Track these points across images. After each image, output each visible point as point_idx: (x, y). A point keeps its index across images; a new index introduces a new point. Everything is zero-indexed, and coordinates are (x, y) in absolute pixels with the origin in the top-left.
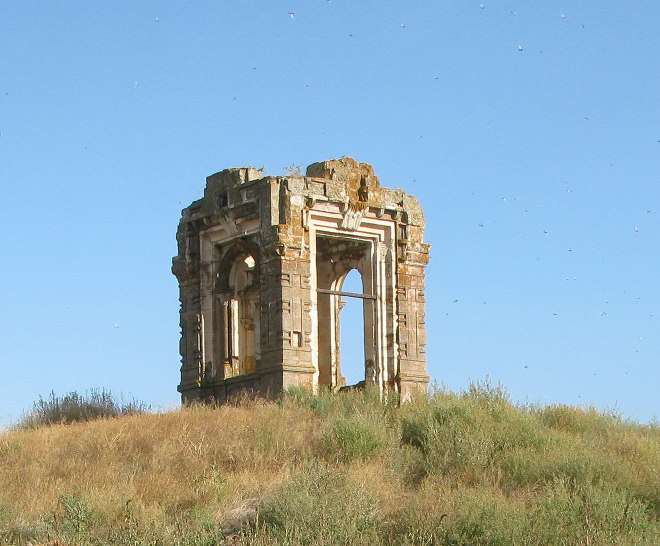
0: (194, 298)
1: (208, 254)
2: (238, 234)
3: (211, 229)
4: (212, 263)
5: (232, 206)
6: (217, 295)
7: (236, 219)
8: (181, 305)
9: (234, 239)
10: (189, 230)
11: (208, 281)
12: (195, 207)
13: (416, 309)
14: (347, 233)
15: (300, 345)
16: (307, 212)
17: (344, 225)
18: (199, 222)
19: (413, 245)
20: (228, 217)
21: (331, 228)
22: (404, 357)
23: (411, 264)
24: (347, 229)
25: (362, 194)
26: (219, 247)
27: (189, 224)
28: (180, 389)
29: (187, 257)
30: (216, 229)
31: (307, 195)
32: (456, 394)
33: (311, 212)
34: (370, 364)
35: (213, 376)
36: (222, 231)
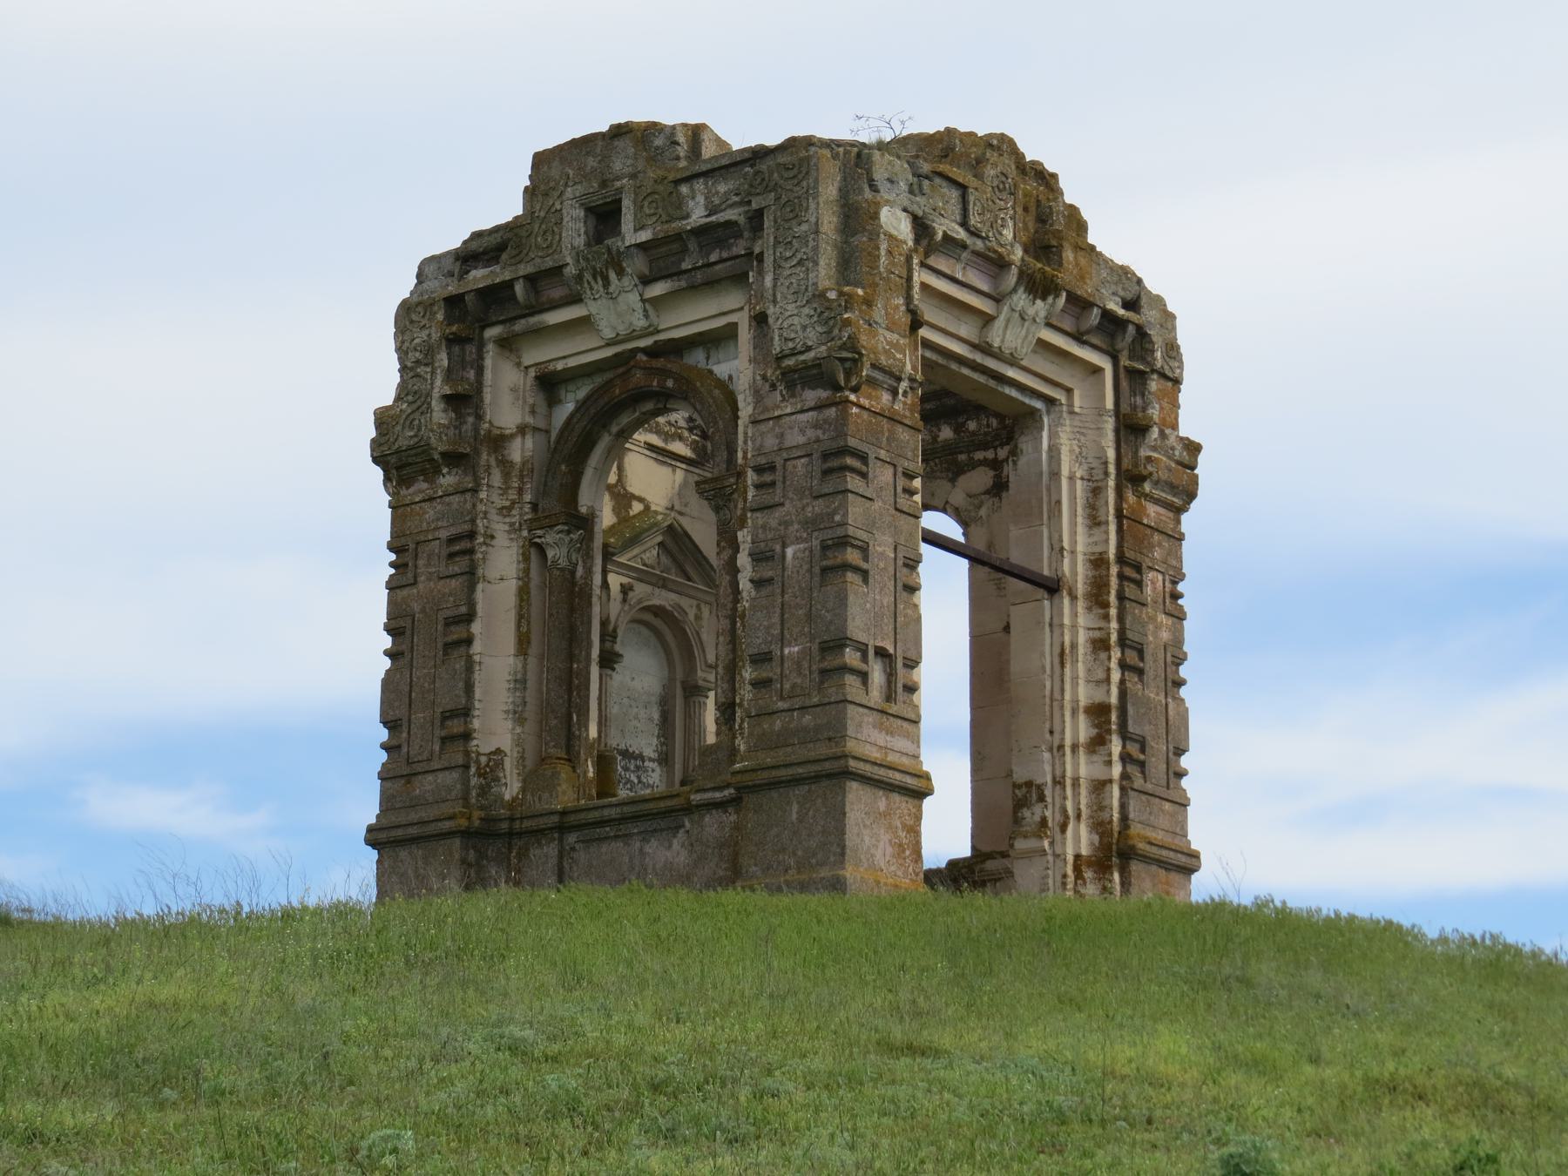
0: (451, 540)
1: (507, 396)
3: (533, 320)
4: (522, 430)
5: (644, 236)
6: (539, 532)
7: (646, 281)
8: (392, 565)
9: (616, 355)
11: (505, 491)
12: (482, 249)
13: (1165, 635)
14: (991, 363)
15: (890, 697)
17: (995, 338)
18: (496, 295)
20: (621, 273)
22: (1138, 782)
23: (1157, 493)
24: (997, 355)
26: (549, 384)
27: (453, 302)
31: (920, 214)
35: (507, 797)
36: (585, 323)
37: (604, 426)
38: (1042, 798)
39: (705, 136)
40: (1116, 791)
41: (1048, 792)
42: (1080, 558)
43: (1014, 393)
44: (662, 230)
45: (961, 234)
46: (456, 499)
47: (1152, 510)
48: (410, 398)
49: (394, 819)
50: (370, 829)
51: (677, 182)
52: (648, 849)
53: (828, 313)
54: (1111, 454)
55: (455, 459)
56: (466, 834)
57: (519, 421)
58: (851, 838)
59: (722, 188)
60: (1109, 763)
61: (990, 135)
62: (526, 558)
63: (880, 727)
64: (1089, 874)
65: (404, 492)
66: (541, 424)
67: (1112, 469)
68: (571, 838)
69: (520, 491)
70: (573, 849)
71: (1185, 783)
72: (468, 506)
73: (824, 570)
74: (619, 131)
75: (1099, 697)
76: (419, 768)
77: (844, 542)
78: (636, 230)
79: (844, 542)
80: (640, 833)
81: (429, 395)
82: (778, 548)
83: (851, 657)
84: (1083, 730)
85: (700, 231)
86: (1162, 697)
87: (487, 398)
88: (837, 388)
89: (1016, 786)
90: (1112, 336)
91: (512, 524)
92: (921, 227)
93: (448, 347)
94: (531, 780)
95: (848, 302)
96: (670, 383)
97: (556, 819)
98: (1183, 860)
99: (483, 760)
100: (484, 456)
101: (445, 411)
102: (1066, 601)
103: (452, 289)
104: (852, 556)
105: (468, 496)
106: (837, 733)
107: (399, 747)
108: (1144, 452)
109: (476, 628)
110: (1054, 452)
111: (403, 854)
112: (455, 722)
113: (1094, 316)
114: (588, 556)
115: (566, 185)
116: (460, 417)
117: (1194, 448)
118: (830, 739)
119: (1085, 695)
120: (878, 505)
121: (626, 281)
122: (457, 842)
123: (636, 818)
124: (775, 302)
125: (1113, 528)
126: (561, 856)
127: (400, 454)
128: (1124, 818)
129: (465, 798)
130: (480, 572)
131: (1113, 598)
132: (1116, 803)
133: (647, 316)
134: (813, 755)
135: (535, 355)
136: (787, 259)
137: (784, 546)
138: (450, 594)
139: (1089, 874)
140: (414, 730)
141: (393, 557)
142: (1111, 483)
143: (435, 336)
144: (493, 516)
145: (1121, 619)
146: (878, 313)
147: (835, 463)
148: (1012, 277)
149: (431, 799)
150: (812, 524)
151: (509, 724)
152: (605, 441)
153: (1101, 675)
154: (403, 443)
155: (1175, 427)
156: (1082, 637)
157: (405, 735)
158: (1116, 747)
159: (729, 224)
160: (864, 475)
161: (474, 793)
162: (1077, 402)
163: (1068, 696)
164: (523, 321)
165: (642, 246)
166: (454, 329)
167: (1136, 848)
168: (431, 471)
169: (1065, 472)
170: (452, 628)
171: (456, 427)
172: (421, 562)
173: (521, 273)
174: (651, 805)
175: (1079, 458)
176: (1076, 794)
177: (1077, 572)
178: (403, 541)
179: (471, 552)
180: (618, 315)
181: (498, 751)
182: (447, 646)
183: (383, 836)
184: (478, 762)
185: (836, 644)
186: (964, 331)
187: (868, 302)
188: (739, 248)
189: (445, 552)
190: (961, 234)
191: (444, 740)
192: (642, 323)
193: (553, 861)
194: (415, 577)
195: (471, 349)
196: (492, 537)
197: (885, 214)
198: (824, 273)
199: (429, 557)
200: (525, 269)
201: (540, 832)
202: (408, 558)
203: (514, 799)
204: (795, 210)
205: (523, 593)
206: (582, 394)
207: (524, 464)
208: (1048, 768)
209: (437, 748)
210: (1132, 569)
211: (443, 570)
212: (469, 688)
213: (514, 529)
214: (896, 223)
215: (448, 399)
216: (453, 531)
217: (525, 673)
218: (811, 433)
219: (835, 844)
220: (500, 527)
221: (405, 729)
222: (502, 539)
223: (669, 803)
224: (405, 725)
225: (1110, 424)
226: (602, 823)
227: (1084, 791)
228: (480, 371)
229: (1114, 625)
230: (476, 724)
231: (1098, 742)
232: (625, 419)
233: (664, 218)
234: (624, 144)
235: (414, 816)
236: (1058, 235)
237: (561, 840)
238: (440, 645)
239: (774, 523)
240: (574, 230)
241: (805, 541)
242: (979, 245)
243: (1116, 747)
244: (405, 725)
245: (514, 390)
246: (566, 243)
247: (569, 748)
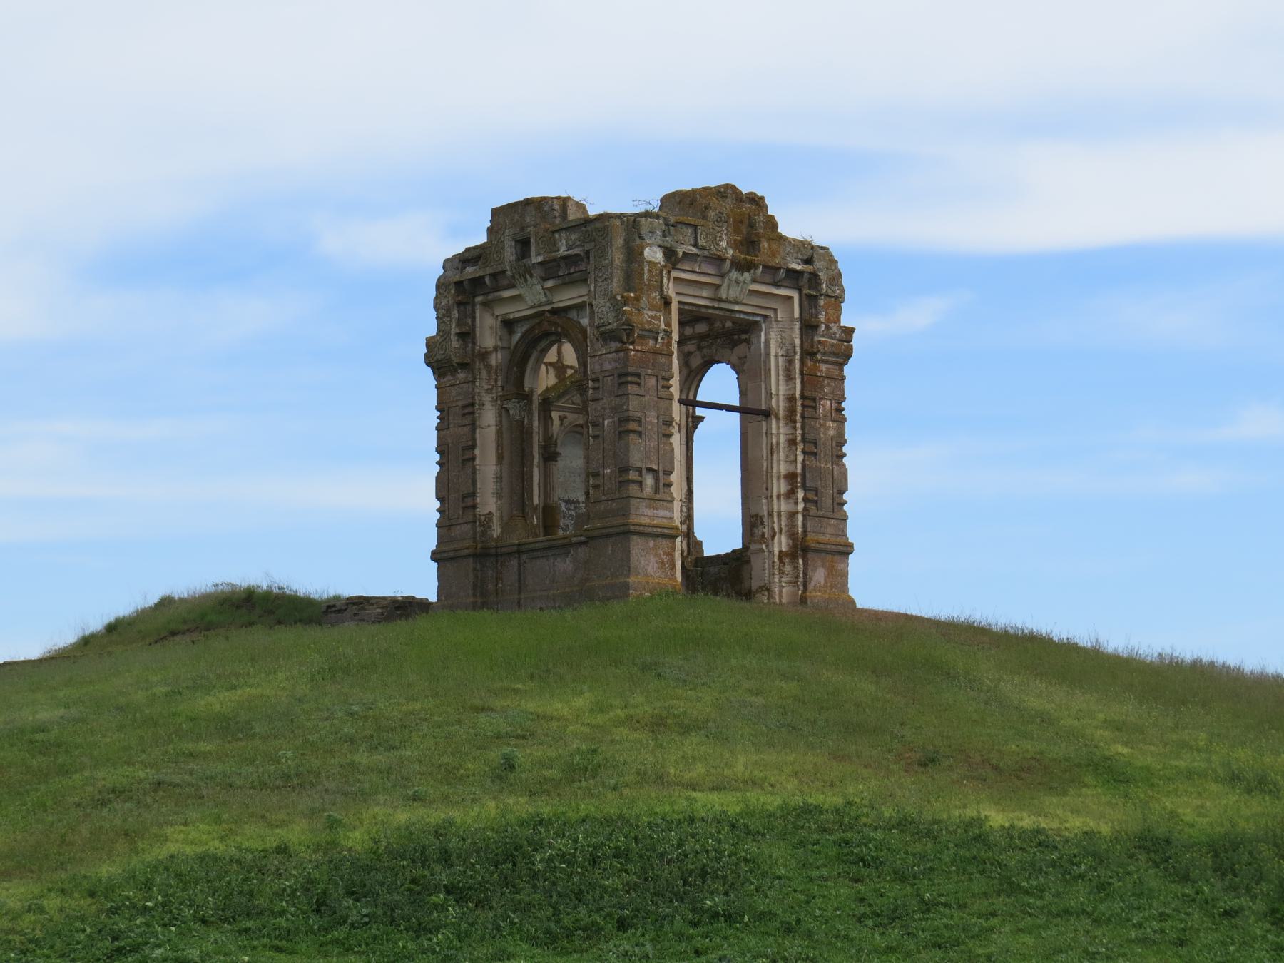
0: (464, 407)
1: (488, 335)
2: (547, 304)
3: (497, 294)
4: (496, 349)
5: (540, 259)
7: (544, 280)
10: (458, 293)
11: (489, 380)
12: (469, 257)
13: (832, 432)
14: (724, 306)
15: (656, 491)
16: (669, 273)
18: (477, 282)
19: (828, 327)
20: (531, 276)
21: (701, 299)
22: (813, 511)
24: (727, 301)
25: (750, 243)
26: (509, 324)
27: (459, 284)
28: (435, 556)
29: (453, 338)
30: (506, 294)
32: (1267, 798)
33: (674, 274)
34: (752, 522)
36: (518, 298)
38: (762, 523)
39: (569, 204)
40: (800, 518)
41: (765, 520)
42: (781, 398)
43: (742, 316)
45: (695, 250)
46: (465, 386)
47: (824, 367)
50: (433, 553)
51: (553, 232)
53: (617, 308)
54: (797, 342)
55: (463, 366)
56: (474, 556)
58: (633, 562)
59: (573, 237)
60: (796, 503)
61: (720, 186)
62: (500, 415)
63: (649, 507)
64: (787, 561)
66: (505, 345)
67: (798, 349)
68: (524, 557)
71: (845, 508)
73: (620, 432)
74: (528, 202)
75: (792, 469)
76: (454, 522)
77: (628, 419)
79: (628, 419)
83: (633, 475)
84: (784, 487)
85: (565, 258)
86: (829, 465)
87: (478, 333)
88: (624, 343)
89: (752, 517)
90: (797, 280)
92: (669, 253)
94: (506, 528)
95: (626, 301)
98: (845, 549)
102: (774, 421)
103: (457, 278)
104: (632, 426)
106: (626, 514)
108: (816, 338)
109: (477, 452)
110: (767, 342)
111: (448, 564)
113: (782, 273)
114: (530, 413)
117: (849, 331)
119: (784, 469)
120: (647, 398)
121: (534, 280)
125: (798, 381)
128: (805, 531)
129: (475, 538)
131: (798, 417)
132: (800, 523)
134: (615, 523)
135: (501, 310)
139: (787, 561)
142: (798, 357)
144: (483, 394)
145: (803, 428)
146: (644, 302)
147: (623, 380)
148: (727, 265)
150: (615, 409)
152: (535, 354)
153: (792, 458)
154: (439, 357)
155: (838, 320)
156: (782, 439)
158: (800, 494)
159: (576, 255)
160: (639, 384)
162: (779, 315)
163: (775, 470)
167: (822, 545)
169: (773, 352)
175: (781, 345)
176: (779, 520)
177: (779, 405)
179: (473, 413)
180: (529, 297)
181: (490, 513)
183: (438, 556)
185: (625, 469)
186: (705, 294)
187: (637, 299)
190: (695, 250)
192: (544, 299)
193: (516, 569)
195: (469, 308)
197: (647, 252)
198: (616, 286)
200: (489, 271)
201: (510, 554)
204: (602, 253)
205: (499, 433)
206: (524, 329)
208: (765, 508)
210: (810, 401)
213: (494, 401)
214: (654, 254)
215: (458, 335)
219: (625, 565)
220: (487, 399)
222: (488, 406)
225: (797, 326)
226: (536, 550)
227: (783, 518)
228: (474, 319)
229: (799, 431)
230: (478, 500)
231: (791, 493)
232: (543, 344)
234: (530, 209)
235: (452, 547)
236: (758, 235)
240: (510, 253)
242: (706, 253)
243: (800, 494)
245: (491, 328)
246: (506, 259)
247: (523, 511)
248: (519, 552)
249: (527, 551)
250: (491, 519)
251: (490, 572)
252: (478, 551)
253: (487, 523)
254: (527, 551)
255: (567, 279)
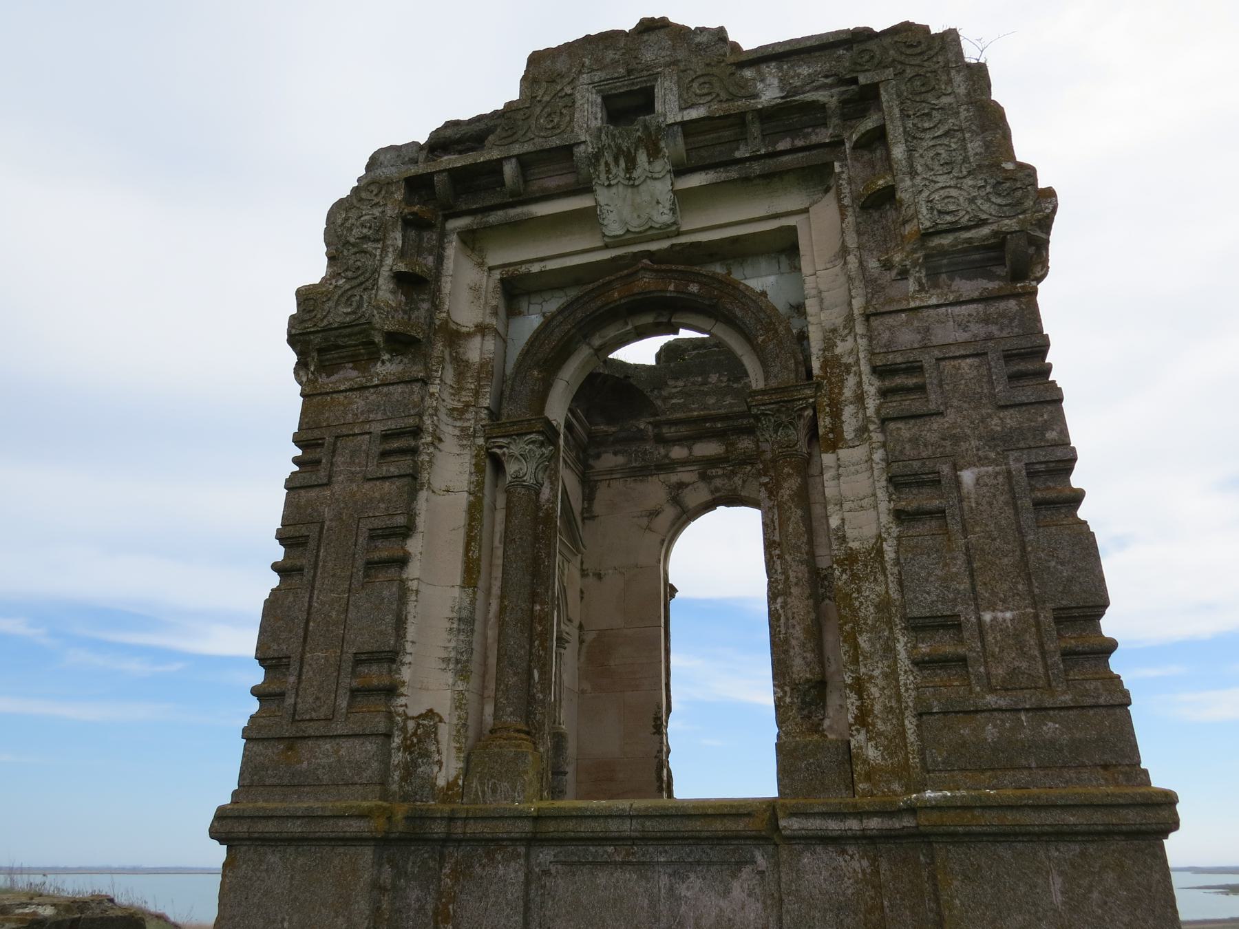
0: (386, 436)
1: (466, 290)
3: (514, 212)
4: (481, 329)
6: (502, 441)
7: (680, 171)
8: (296, 461)
9: (613, 259)
11: (458, 390)
20: (654, 153)
35: (441, 782)
36: (589, 218)
37: (585, 337)
44: (717, 109)
46: (399, 389)
48: (350, 274)
49: (247, 806)
50: (221, 815)
52: (682, 890)
55: (401, 343)
56: (383, 842)
57: (480, 320)
59: (805, 71)
62: (478, 469)
65: (323, 379)
68: (545, 856)
69: (477, 394)
70: (546, 872)
72: (416, 398)
78: (681, 109)
80: (669, 863)
81: (376, 271)
82: (946, 469)
85: (767, 115)
91: (463, 429)
93: (404, 229)
94: (480, 751)
96: (694, 288)
97: (528, 827)
98: (1132, 818)
99: (411, 725)
100: (439, 346)
101: (393, 292)
105: (416, 387)
107: (281, 695)
109: (414, 545)
112: (375, 670)
115: (580, 73)
116: (412, 304)
118: (1105, 767)
121: (660, 166)
122: (367, 854)
123: (664, 839)
124: (913, 173)
126: (527, 883)
127: (322, 335)
130: (425, 476)
133: (673, 210)
135: (500, 256)
136: (925, 130)
137: (956, 467)
138: (382, 500)
140: (308, 673)
141: (299, 452)
143: (391, 211)
149: (326, 779)
150: (1005, 442)
151: (449, 677)
157: (292, 679)
161: (396, 776)
164: (500, 213)
165: (687, 127)
166: (416, 209)
168: (365, 354)
170: (379, 543)
171: (405, 312)
172: (339, 459)
173: (516, 152)
174: (698, 825)
178: (317, 433)
179: (414, 451)
180: (638, 205)
181: (430, 714)
182: (370, 565)
183: (241, 829)
184: (404, 729)
188: (824, 136)
189: (377, 448)
191: (354, 693)
193: (514, 893)
194: (330, 477)
195: (430, 237)
196: (440, 440)
199: (353, 454)
201: (493, 844)
202: (317, 454)
203: (450, 786)
205: (474, 510)
207: (482, 365)
209: (343, 703)
211: (372, 469)
212: (400, 624)
213: (465, 435)
215: (400, 279)
216: (392, 425)
217: (472, 613)
218: (977, 329)
220: (449, 430)
221: (294, 670)
222: (450, 444)
223: (731, 825)
224: (294, 666)
228: (440, 259)
230: (406, 674)
233: (723, 96)
237: (527, 856)
238: (360, 563)
239: (933, 437)
240: (588, 114)
241: (995, 462)
244: (294, 666)
245: (475, 289)
248: (534, 841)
249: (561, 841)
250: (432, 733)
251: (414, 894)
252: (401, 826)
253: (420, 740)
254: (561, 841)
255: (757, 168)
